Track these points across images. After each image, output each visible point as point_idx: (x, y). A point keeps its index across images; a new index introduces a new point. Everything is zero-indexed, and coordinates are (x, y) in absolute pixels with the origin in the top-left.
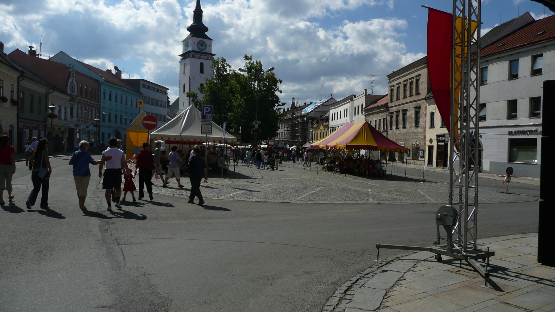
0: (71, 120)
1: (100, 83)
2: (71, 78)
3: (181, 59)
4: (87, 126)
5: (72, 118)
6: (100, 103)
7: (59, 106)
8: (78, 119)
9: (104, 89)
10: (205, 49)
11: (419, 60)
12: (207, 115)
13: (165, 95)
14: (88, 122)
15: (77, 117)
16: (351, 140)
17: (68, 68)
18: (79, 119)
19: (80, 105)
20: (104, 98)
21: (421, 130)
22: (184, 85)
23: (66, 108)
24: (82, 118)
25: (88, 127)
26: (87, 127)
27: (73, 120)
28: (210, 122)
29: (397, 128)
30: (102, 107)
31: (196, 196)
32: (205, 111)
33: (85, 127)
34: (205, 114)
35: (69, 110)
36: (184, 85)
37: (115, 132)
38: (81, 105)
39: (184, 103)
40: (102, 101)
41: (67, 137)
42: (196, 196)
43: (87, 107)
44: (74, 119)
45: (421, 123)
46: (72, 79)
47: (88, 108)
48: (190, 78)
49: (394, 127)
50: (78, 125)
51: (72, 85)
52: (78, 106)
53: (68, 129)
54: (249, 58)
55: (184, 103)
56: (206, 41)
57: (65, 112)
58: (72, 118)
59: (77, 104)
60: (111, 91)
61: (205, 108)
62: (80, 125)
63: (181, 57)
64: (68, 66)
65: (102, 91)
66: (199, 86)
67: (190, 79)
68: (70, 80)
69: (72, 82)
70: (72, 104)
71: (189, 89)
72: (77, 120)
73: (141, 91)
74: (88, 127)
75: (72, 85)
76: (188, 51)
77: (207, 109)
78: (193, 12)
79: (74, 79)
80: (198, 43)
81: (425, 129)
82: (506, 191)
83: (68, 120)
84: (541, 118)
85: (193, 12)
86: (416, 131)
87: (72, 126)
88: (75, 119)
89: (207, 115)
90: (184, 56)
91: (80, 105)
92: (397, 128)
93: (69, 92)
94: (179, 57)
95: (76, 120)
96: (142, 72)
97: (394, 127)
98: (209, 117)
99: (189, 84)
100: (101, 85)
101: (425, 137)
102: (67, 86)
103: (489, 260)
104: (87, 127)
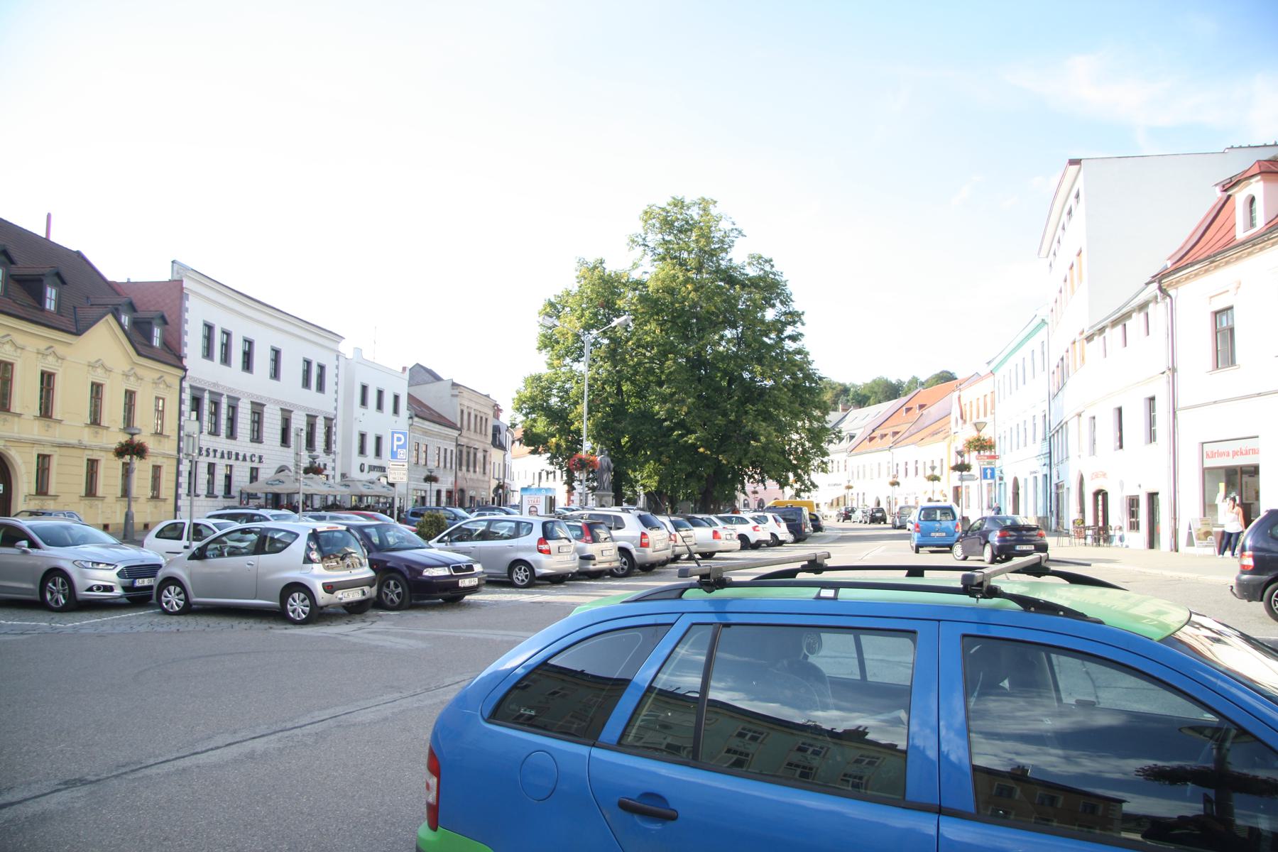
11: (1018, 828)
12: (399, 450)
16: (1122, 709)
21: (487, 479)
22: (49, 217)
28: (403, 465)
29: (468, 470)
31: (1001, 684)
32: (396, 443)
34: (395, 449)
36: (49, 217)
42: (1001, 684)
45: (487, 471)
49: (464, 468)
61: (396, 436)
66: (806, 350)
77: (399, 439)
81: (490, 479)
86: (483, 478)
89: (399, 450)
92: (468, 470)
96: (1188, 783)
97: (464, 468)
98: (402, 452)
101: (490, 488)
103: (865, 639)
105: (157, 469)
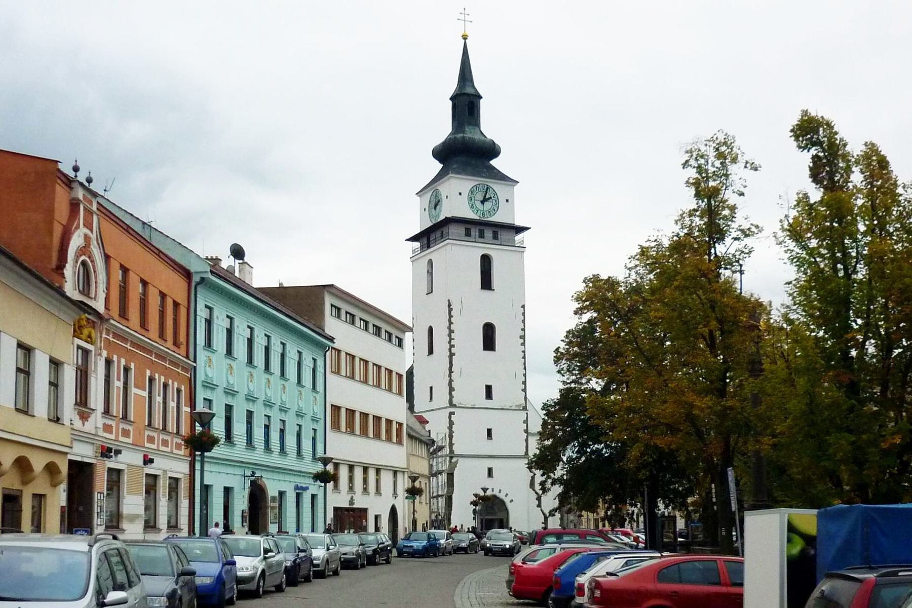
0: (78, 424)
1: (196, 279)
2: (83, 230)
3: (414, 251)
4: (145, 456)
5: (84, 417)
6: (195, 361)
7: (20, 345)
8: (109, 422)
9: (206, 306)
10: (495, 210)
13: (397, 349)
14: (151, 440)
15: (107, 412)
17: (69, 182)
18: (113, 423)
19: (119, 362)
20: (209, 343)
22: (431, 330)
23: (55, 364)
24: (125, 417)
25: (152, 461)
26: (148, 461)
27: (89, 426)
30: (200, 377)
33: (140, 462)
35: (69, 376)
36: (431, 330)
37: (248, 484)
38: (123, 362)
39: (431, 388)
40: (202, 355)
41: (64, 504)
43: (148, 373)
44: (91, 419)
46: (86, 236)
47: (151, 380)
48: (449, 305)
50: (110, 450)
51: (84, 263)
52: (108, 362)
53: (64, 469)
54: (813, 151)
55: (431, 388)
56: (498, 187)
57: (51, 383)
58: (84, 417)
59: (105, 354)
60: (231, 319)
62: (118, 452)
63: (417, 245)
64: (72, 174)
65: (202, 313)
67: (450, 310)
68: (76, 242)
69: (84, 250)
70: (86, 352)
71: (450, 342)
72: (108, 429)
73: (329, 331)
74: (152, 461)
75: (84, 263)
76: (442, 218)
78: (450, 99)
79: (93, 236)
80: (472, 191)
82: (164, 548)
83: (66, 422)
84: (350, 505)
85: (450, 99)
87: (84, 452)
88: (97, 420)
90: (425, 241)
91: (119, 362)
93: (71, 289)
94: (410, 243)
95: (100, 425)
99: (448, 324)
100: (199, 288)
102: (60, 267)
104: (148, 461)
105: (313, 497)
